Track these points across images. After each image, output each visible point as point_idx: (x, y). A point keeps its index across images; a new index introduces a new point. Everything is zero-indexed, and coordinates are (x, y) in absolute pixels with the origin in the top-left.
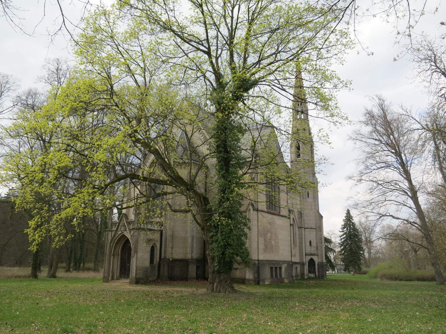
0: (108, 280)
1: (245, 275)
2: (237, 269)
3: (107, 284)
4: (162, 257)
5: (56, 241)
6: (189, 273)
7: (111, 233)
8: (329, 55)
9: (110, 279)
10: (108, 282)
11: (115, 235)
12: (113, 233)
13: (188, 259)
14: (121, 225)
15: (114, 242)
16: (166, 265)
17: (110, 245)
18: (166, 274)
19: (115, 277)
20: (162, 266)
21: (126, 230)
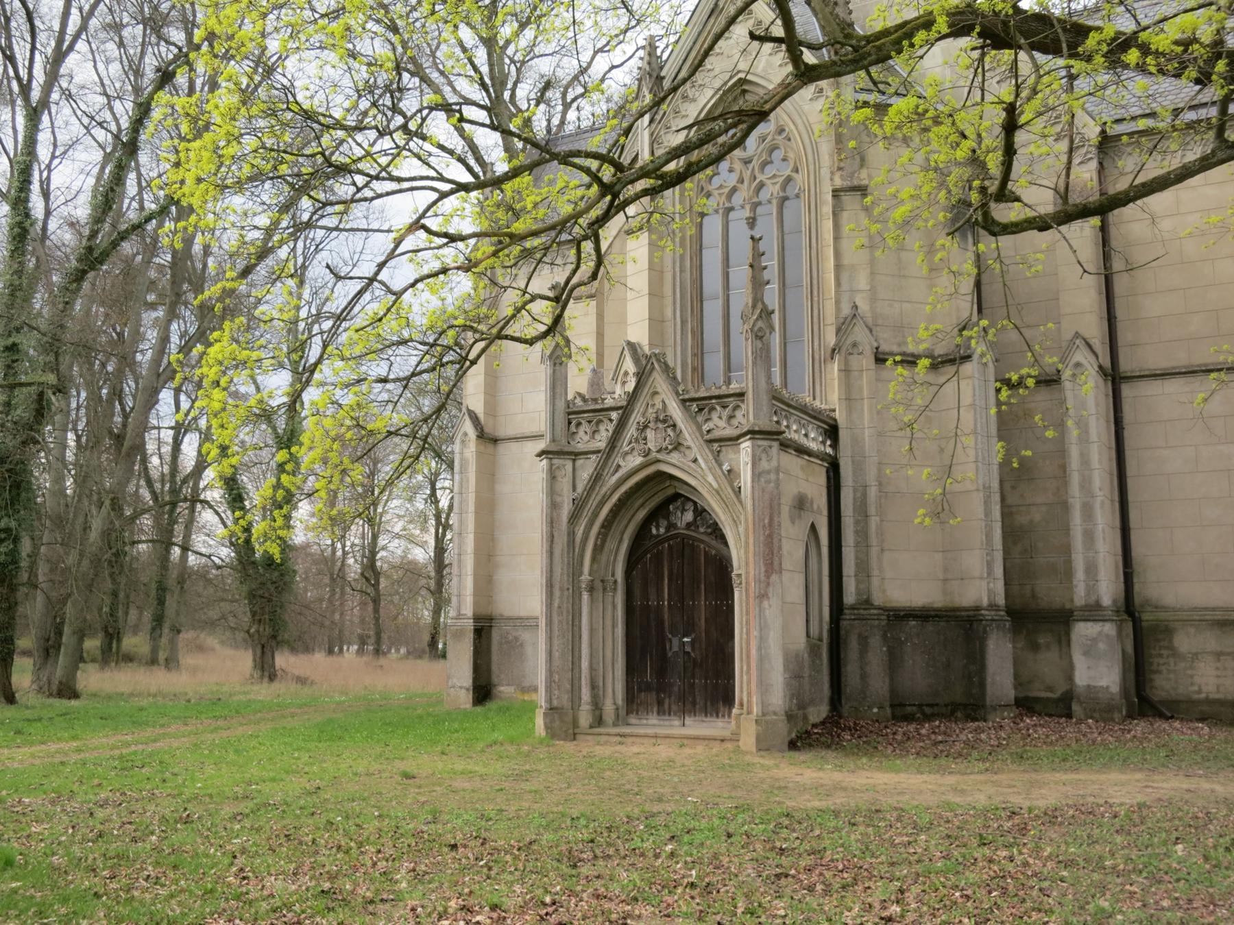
0: (575, 724)
1: (1070, 678)
2: (1195, 656)
3: (569, 747)
4: (850, 597)
5: (969, 441)
6: (989, 680)
7: (569, 465)
8: (155, 190)
9: (585, 719)
10: (573, 734)
11: (597, 478)
12: (587, 469)
13: (977, 609)
14: (636, 418)
15: (595, 515)
16: (875, 641)
17: (571, 534)
18: (879, 685)
19: (609, 708)
20: (853, 646)
21: (677, 446)
